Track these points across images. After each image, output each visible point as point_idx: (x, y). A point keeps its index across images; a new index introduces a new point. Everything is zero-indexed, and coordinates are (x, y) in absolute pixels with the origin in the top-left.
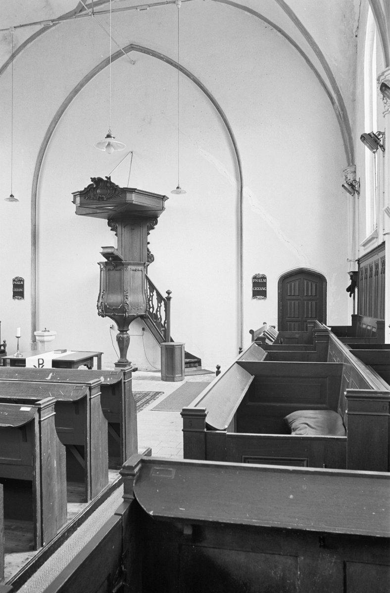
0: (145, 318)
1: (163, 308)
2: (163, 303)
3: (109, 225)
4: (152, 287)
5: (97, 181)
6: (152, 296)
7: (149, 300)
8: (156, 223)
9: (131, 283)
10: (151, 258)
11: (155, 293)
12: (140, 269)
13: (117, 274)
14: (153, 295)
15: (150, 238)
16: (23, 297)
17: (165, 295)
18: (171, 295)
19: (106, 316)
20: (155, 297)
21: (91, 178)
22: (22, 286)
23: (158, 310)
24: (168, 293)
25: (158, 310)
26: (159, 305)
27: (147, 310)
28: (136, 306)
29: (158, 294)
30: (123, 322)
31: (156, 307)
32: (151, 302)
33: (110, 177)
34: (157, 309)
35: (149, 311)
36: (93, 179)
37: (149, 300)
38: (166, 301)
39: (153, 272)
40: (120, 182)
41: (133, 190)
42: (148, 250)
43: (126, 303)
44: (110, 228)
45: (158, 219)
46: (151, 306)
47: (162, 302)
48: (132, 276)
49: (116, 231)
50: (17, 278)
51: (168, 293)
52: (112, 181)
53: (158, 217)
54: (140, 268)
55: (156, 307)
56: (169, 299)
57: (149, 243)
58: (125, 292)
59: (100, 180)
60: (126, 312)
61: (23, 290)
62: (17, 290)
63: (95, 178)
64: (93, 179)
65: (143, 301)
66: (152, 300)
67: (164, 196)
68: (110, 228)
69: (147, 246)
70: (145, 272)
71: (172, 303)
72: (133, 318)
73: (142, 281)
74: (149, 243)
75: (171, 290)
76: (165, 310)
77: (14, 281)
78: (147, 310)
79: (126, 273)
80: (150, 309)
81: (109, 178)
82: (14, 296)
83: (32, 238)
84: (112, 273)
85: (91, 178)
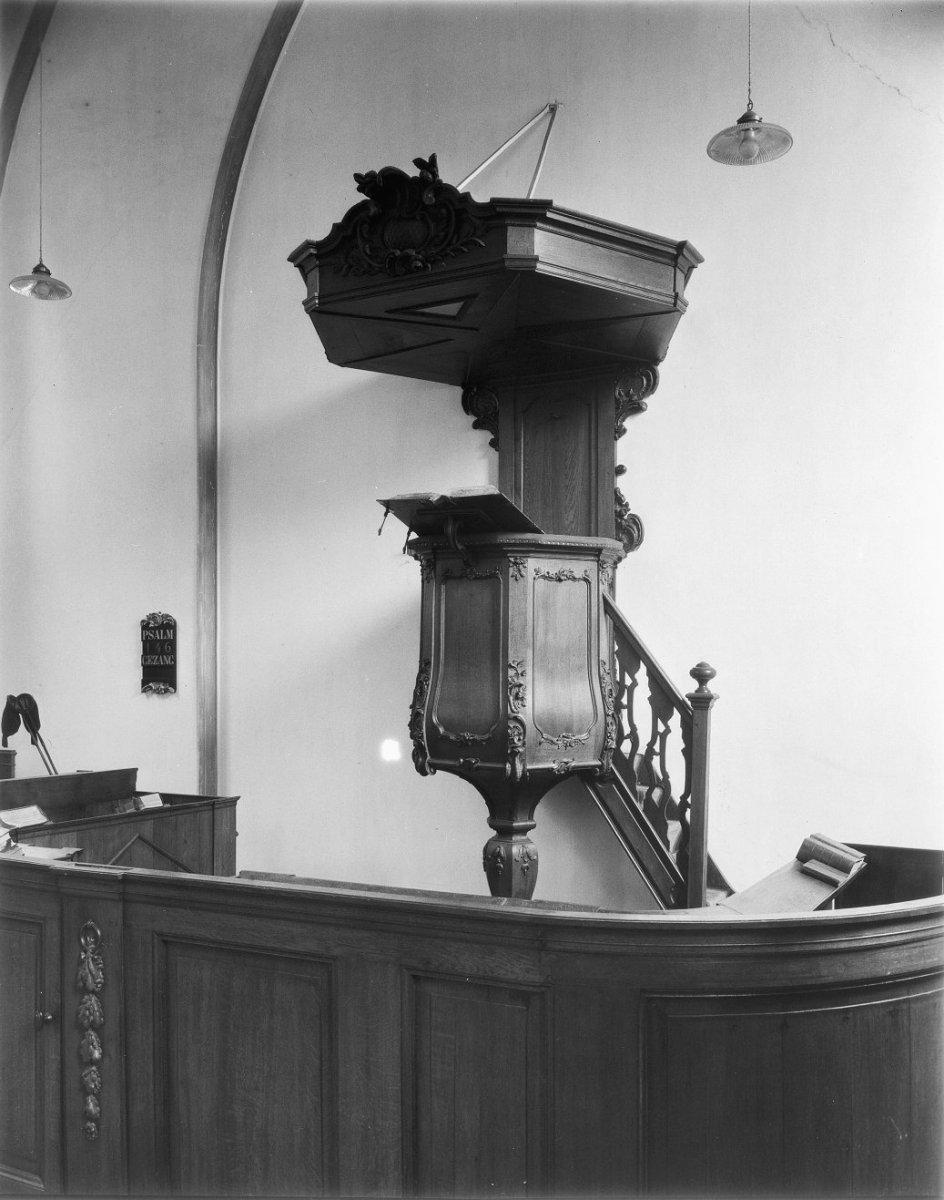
0: (601, 779)
1: (675, 742)
2: (676, 720)
3: (468, 405)
4: (630, 651)
5: (380, 186)
6: (664, 736)
7: (618, 707)
8: (652, 387)
9: (540, 631)
10: (629, 532)
11: (642, 675)
12: (578, 574)
13: (480, 594)
14: (668, 731)
15: (624, 450)
16: (175, 689)
17: (684, 686)
18: (712, 686)
19: (435, 768)
20: (643, 693)
21: (357, 177)
22: (169, 648)
23: (657, 748)
24: (701, 674)
25: (657, 748)
26: (661, 728)
27: (605, 748)
28: (557, 729)
29: (657, 681)
30: (509, 798)
31: (645, 737)
32: (625, 712)
33: (433, 158)
34: (651, 745)
35: (618, 750)
36: (365, 182)
37: (617, 699)
38: (695, 713)
39: (642, 590)
40: (477, 179)
41: (533, 212)
42: (619, 499)
43: (516, 719)
44: (472, 419)
45: (661, 368)
46: (627, 730)
47: (670, 715)
48: (544, 597)
49: (494, 431)
50: (153, 617)
51: (701, 674)
52: (446, 175)
53: (657, 360)
54: (580, 567)
55: (645, 737)
56: (702, 701)
57: (620, 470)
58: (511, 672)
59: (392, 176)
60: (515, 754)
61: (174, 660)
62: (155, 661)
63: (371, 175)
64: (365, 182)
65: (589, 708)
66: (630, 707)
67: (681, 246)
68: (472, 419)
69: (613, 482)
70: (604, 588)
71: (718, 720)
72: (541, 784)
73: (590, 627)
74: (620, 470)
75: (712, 663)
76: (684, 751)
77: (145, 626)
78: (605, 748)
79: (514, 589)
80: (620, 738)
81: (428, 166)
82: (145, 682)
83: (199, 475)
84: (461, 591)
85: (357, 177)
